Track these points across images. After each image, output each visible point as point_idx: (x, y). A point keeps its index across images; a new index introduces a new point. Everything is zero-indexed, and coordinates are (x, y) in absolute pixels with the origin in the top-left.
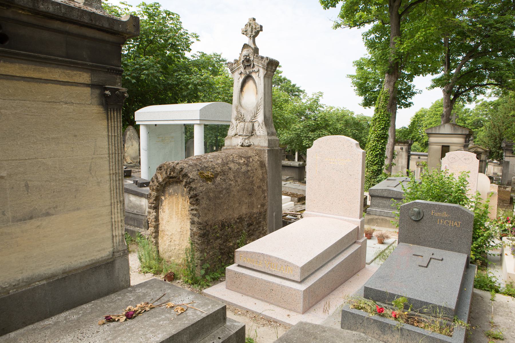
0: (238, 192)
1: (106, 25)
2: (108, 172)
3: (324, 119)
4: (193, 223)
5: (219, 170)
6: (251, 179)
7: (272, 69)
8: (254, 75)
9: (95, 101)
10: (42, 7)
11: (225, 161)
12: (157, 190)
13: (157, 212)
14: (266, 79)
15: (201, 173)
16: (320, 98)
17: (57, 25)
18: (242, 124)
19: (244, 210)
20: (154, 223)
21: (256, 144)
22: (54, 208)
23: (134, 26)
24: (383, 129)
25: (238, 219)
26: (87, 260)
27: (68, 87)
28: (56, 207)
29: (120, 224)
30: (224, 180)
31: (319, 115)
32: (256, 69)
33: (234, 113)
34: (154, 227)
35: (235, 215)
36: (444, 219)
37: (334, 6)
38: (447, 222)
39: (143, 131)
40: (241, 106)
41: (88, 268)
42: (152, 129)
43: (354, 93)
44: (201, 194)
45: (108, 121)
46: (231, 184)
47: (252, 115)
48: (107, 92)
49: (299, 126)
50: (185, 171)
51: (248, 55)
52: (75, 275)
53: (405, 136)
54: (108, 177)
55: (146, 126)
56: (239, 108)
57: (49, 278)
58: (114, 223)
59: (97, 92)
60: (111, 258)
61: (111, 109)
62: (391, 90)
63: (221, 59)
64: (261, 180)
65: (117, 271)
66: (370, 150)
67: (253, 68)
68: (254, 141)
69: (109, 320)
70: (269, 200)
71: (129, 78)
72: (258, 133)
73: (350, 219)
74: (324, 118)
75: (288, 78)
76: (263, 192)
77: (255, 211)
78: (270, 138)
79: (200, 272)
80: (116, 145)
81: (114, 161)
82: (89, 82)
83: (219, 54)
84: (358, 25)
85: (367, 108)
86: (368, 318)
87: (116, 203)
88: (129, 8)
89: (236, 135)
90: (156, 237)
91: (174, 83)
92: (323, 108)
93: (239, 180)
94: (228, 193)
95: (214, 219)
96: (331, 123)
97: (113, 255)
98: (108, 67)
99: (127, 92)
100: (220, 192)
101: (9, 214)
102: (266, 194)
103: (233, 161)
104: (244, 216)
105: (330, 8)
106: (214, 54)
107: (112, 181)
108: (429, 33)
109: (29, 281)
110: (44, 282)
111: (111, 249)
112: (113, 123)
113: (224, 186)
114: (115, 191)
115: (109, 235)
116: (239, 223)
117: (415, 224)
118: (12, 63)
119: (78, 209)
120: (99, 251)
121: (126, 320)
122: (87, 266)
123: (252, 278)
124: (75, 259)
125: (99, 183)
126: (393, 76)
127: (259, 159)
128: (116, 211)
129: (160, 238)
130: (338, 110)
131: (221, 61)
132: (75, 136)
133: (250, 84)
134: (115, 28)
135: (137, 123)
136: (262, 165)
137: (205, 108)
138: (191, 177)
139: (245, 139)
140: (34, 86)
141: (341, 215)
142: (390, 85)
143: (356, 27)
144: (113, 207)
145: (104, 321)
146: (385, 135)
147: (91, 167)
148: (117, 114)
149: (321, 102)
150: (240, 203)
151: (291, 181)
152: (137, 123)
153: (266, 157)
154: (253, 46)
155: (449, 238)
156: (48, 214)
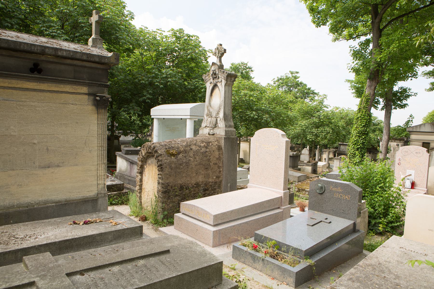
0: (196, 166)
1: (97, 60)
2: (97, 145)
3: (327, 117)
4: (159, 183)
5: (182, 149)
6: (208, 157)
7: (231, 80)
8: (219, 84)
9: (90, 103)
10: (60, 53)
11: (188, 144)
12: (142, 161)
13: (142, 176)
14: (227, 87)
15: (167, 151)
16: (325, 100)
17: (69, 61)
18: (210, 119)
19: (200, 179)
20: (139, 183)
21: (218, 133)
22: (62, 163)
24: (364, 126)
26: (80, 196)
27: (74, 96)
28: (64, 163)
29: (103, 177)
30: (185, 157)
32: (220, 80)
33: (206, 111)
34: (139, 186)
35: (193, 182)
36: (339, 193)
37: (324, 24)
39: (155, 122)
40: (210, 106)
41: (81, 201)
42: (163, 121)
46: (190, 160)
47: (216, 113)
48: (98, 98)
49: (304, 123)
50: (156, 148)
51: (215, 70)
52: (72, 203)
53: (399, 134)
54: (96, 148)
55: (158, 119)
56: (209, 108)
57: (57, 203)
59: (92, 98)
60: (96, 196)
62: (371, 93)
64: (217, 159)
65: (99, 206)
67: (218, 79)
68: (216, 131)
69: (75, 223)
70: (224, 175)
71: (158, 84)
72: (219, 126)
73: (277, 190)
75: (304, 82)
76: (219, 167)
77: (210, 180)
78: (227, 129)
79: (160, 217)
81: (101, 138)
82: (87, 92)
83: (245, 63)
84: (353, 38)
86: (246, 251)
88: (163, 33)
89: (206, 126)
90: (140, 193)
91: (192, 87)
92: (327, 108)
93: (197, 157)
95: (174, 182)
97: (97, 195)
98: (99, 83)
99: (111, 98)
100: (181, 164)
101: (37, 164)
102: (221, 170)
103: (195, 144)
105: (322, 26)
106: (242, 63)
108: (403, 44)
109: (46, 202)
110: (54, 204)
111: (97, 192)
112: (101, 116)
113: (184, 161)
115: (95, 183)
116: (196, 187)
117: (320, 196)
118: (43, 83)
119: (77, 165)
120: (88, 192)
121: (83, 224)
122: (80, 199)
123: (187, 222)
124: (73, 194)
125: (90, 151)
127: (218, 144)
128: (101, 168)
129: (142, 193)
130: (344, 110)
132: (77, 123)
133: (216, 91)
134: (103, 61)
135: (152, 117)
136: (219, 148)
137: (194, 107)
138: (160, 153)
139: (211, 129)
140: (55, 95)
143: (352, 40)
145: (72, 223)
146: (366, 131)
147: (86, 141)
149: (325, 103)
150: (197, 174)
152: (152, 117)
153: (222, 143)
154: (219, 64)
155: (342, 207)
156: (58, 166)
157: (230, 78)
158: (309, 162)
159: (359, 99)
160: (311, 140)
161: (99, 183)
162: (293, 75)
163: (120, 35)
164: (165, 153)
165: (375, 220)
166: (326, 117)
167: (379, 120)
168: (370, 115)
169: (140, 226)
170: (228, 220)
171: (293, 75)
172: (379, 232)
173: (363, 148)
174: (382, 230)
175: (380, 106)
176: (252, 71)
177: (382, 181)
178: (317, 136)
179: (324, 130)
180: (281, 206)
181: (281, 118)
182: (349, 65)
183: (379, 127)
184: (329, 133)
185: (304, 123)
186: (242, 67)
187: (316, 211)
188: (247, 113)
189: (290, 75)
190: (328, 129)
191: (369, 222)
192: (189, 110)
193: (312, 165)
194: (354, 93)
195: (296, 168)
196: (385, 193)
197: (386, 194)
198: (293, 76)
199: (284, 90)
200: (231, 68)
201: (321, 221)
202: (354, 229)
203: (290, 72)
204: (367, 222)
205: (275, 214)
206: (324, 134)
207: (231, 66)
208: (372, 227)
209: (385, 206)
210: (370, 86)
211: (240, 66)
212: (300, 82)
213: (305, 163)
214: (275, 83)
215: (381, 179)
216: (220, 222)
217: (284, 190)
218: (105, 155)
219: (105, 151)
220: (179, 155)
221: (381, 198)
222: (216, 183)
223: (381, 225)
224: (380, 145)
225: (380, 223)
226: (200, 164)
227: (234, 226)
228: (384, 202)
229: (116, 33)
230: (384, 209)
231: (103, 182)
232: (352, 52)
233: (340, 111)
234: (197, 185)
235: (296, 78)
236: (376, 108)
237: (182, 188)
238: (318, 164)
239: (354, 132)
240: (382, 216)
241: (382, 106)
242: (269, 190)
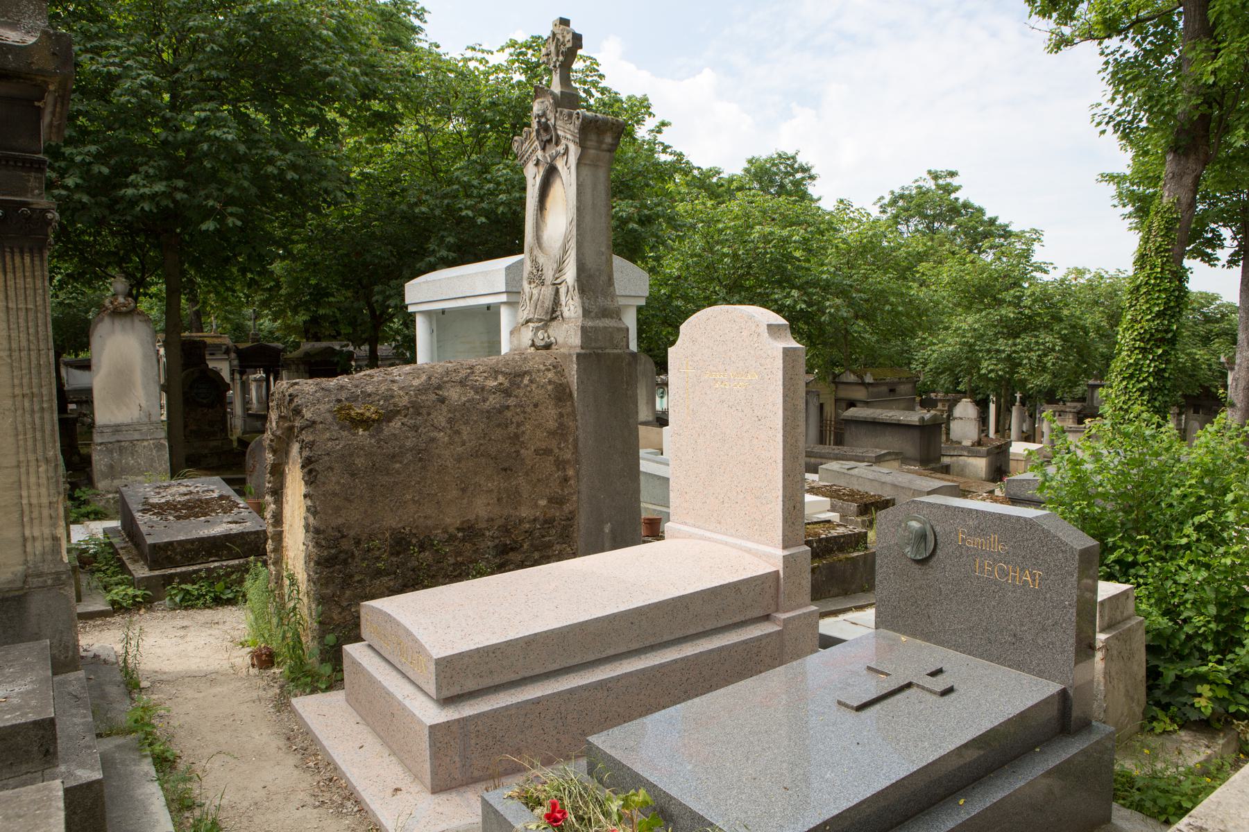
0: (459, 460)
2: (8, 391)
3: (1044, 298)
5: (405, 401)
6: (512, 429)
7: (601, 142)
8: (560, 164)
14: (586, 171)
16: (1036, 246)
19: (481, 508)
23: (54, 54)
24: (1159, 315)
25: (458, 529)
29: (46, 512)
30: (415, 428)
32: (561, 148)
35: (448, 520)
38: (1002, 569)
44: (326, 458)
45: (5, 274)
46: (433, 440)
47: (555, 266)
49: (968, 321)
51: (544, 114)
54: (8, 403)
55: (428, 314)
56: (536, 252)
58: (26, 508)
60: (19, 584)
61: (12, 249)
62: (1184, 201)
63: (796, 166)
64: (552, 434)
66: (1120, 378)
67: (557, 144)
72: (566, 314)
75: (976, 203)
76: (560, 464)
77: (525, 512)
80: (32, 331)
81: (24, 365)
84: (1119, 33)
87: (33, 463)
92: (1046, 272)
93: (465, 430)
94: (421, 460)
97: (25, 582)
102: (571, 473)
104: (483, 525)
106: (780, 156)
107: (19, 412)
111: (21, 568)
113: (408, 444)
114: (29, 436)
115: (13, 533)
126: (1193, 157)
127: (556, 379)
128: (33, 480)
130: (1102, 278)
131: (797, 171)
135: (411, 309)
136: (561, 394)
141: (742, 537)
144: (23, 470)
146: (1167, 331)
148: (32, 261)
149: (1036, 258)
150: (464, 490)
151: (896, 464)
153: (572, 374)
157: (593, 137)
160: (992, 375)
161: (27, 533)
162: (941, 182)
163: (326, 63)
164: (329, 417)
165: (1180, 665)
166: (1042, 300)
167: (1223, 305)
168: (1180, 276)
169: (36, 724)
170: (514, 677)
171: (941, 182)
172: (1194, 716)
173: (1159, 389)
174: (1208, 712)
175: (1223, 254)
176: (812, 178)
177: (1209, 502)
178: (1013, 363)
179: (1037, 343)
180: (777, 611)
181: (888, 307)
182: (1099, 110)
183: (1225, 325)
184: (1053, 350)
185: (968, 321)
186: (782, 167)
187: (905, 633)
188: (773, 297)
189: (931, 184)
190: (1048, 339)
191: (1153, 674)
192: (504, 272)
193: (988, 454)
194: (1130, 216)
195: (932, 466)
196: (1222, 550)
197: (1225, 554)
198: (939, 187)
199: (912, 228)
200: (747, 171)
201: (909, 685)
202: (1064, 717)
203: (929, 172)
204: (1142, 673)
205: (745, 642)
206: (1034, 356)
207: (746, 165)
208: (1167, 693)
209: (1221, 605)
210: (1177, 177)
211: (774, 165)
212: (961, 201)
213: (965, 448)
214: (884, 212)
215: (1203, 493)
216: (471, 685)
217: (785, 547)
218: (48, 427)
219: (47, 416)
220: (390, 421)
221: (1205, 573)
222: (549, 522)
223: (1204, 689)
224: (1229, 382)
225: (1202, 679)
226: (476, 454)
227: (537, 701)
228: (1217, 591)
229: (314, 57)
230: (1218, 619)
231: (47, 531)
232: (1110, 69)
233: (1089, 280)
234: (470, 531)
235: (948, 190)
236: (1210, 260)
237: (400, 543)
238: (1012, 450)
239: (1125, 337)
240: (1209, 647)
241: (1232, 251)
242: (734, 546)
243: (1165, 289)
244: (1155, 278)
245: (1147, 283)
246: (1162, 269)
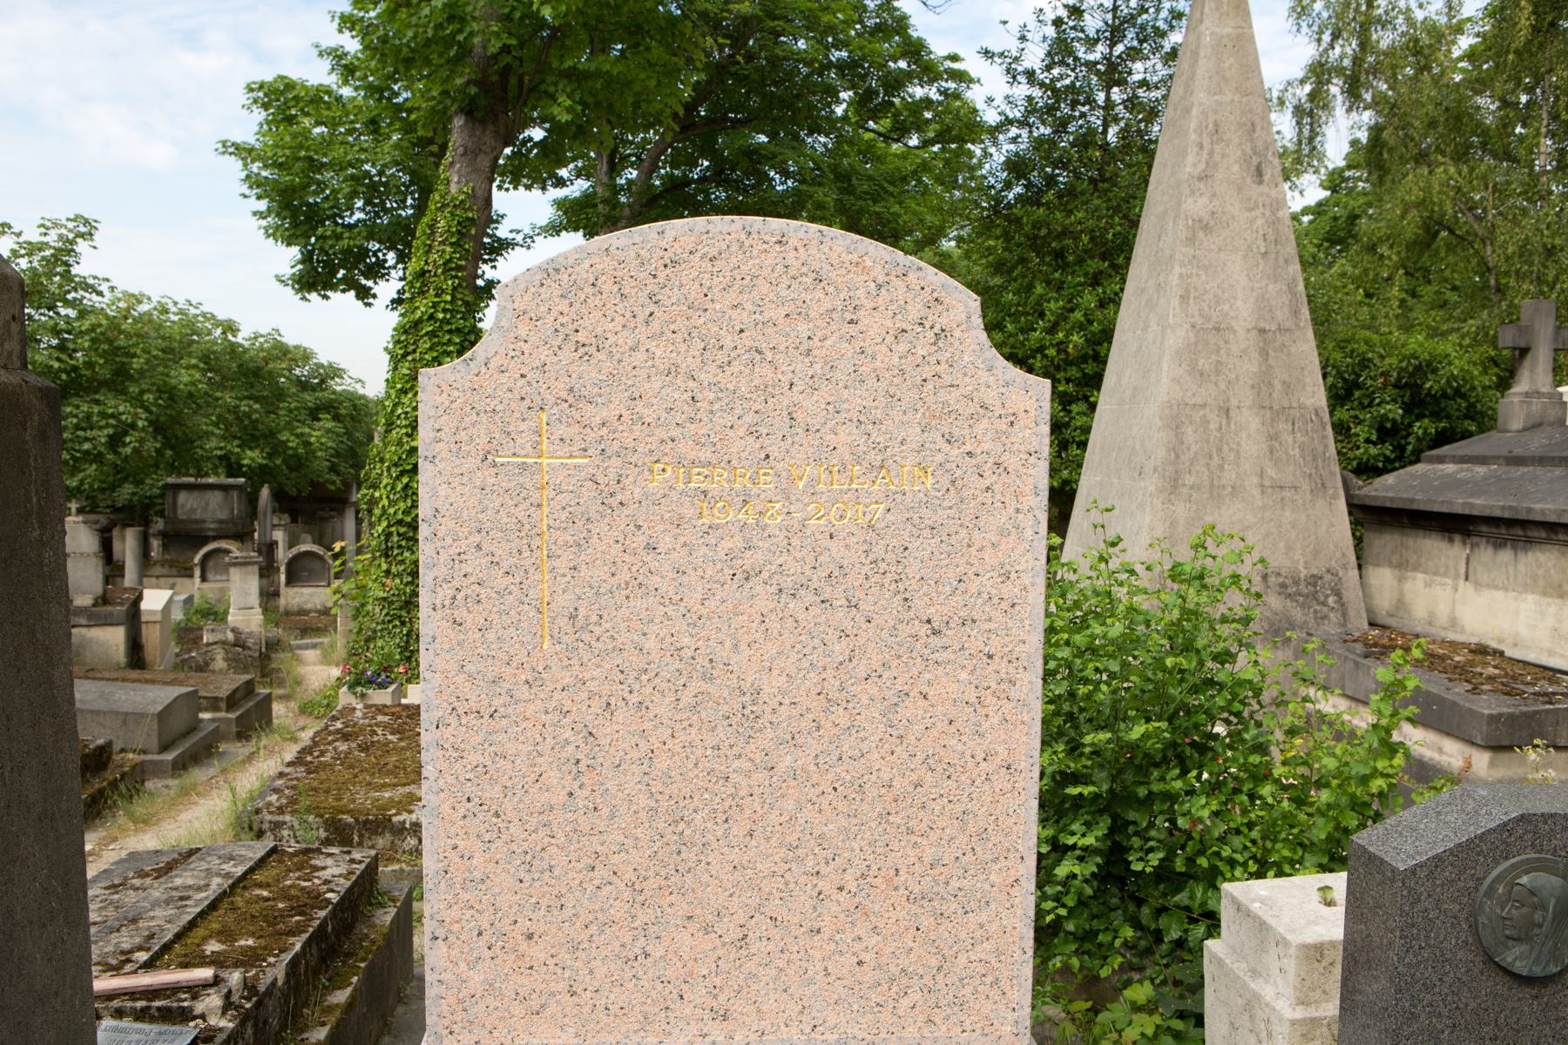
16: (82, 246)
31: (86, 325)
43: (255, 227)
74: (110, 341)
85: (313, 296)
92: (100, 294)
96: (137, 363)
130: (167, 312)
142: (475, 170)
158: (104, 600)
159: (295, 252)
179: (103, 415)
184: (133, 426)
243: (458, 330)
244: (444, 311)
245: (431, 317)
246: (453, 296)
